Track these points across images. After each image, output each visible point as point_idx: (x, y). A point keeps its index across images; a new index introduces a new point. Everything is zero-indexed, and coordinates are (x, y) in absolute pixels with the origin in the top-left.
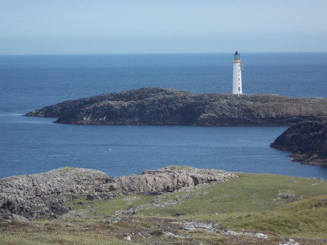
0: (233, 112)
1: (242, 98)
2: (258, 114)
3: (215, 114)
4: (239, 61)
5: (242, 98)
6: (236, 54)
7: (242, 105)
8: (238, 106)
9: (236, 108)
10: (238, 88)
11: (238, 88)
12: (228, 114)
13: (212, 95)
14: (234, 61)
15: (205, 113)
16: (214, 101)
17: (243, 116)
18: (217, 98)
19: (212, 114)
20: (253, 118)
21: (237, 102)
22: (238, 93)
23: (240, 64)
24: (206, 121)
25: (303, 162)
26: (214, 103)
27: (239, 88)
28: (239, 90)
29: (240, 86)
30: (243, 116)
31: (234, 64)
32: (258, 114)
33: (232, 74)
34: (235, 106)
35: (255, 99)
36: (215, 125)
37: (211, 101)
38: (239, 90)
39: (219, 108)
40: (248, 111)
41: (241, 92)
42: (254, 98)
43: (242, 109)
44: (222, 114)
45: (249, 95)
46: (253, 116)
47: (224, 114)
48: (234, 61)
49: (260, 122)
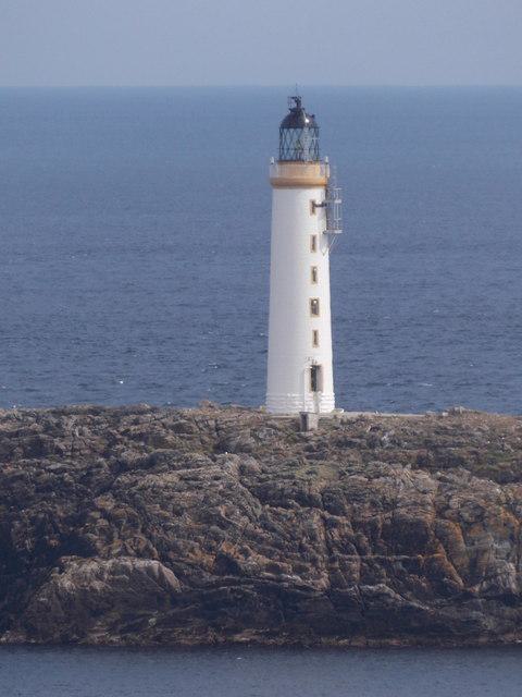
0: (291, 545)
1: (343, 444)
2: (474, 563)
3: (164, 559)
4: (316, 172)
5: (342, 440)
6: (294, 120)
7: (355, 497)
8: (329, 502)
9: (315, 521)
10: (306, 375)
11: (306, 375)
12: (256, 560)
13: (116, 417)
14: (277, 171)
15: (87, 552)
16: (150, 465)
17: (367, 578)
18: (160, 442)
19: (141, 563)
20: (443, 590)
21: (321, 477)
22: (310, 407)
23: (318, 195)
24: (97, 613)
25: (382, 518)
26: (151, 479)
27: (315, 371)
28: (315, 386)
29: (324, 356)
30: (367, 578)
31: (279, 195)
32: (474, 563)
33: (267, 290)
34: (306, 501)
35: (435, 455)
36: (163, 645)
37: (122, 467)
38: (315, 386)
39: (187, 521)
40: (404, 540)
41: (327, 403)
42: (427, 444)
43: (355, 525)
44: (209, 559)
45: (389, 419)
46: (435, 574)
47: (227, 564)
48: (277, 171)
49: (490, 623)
